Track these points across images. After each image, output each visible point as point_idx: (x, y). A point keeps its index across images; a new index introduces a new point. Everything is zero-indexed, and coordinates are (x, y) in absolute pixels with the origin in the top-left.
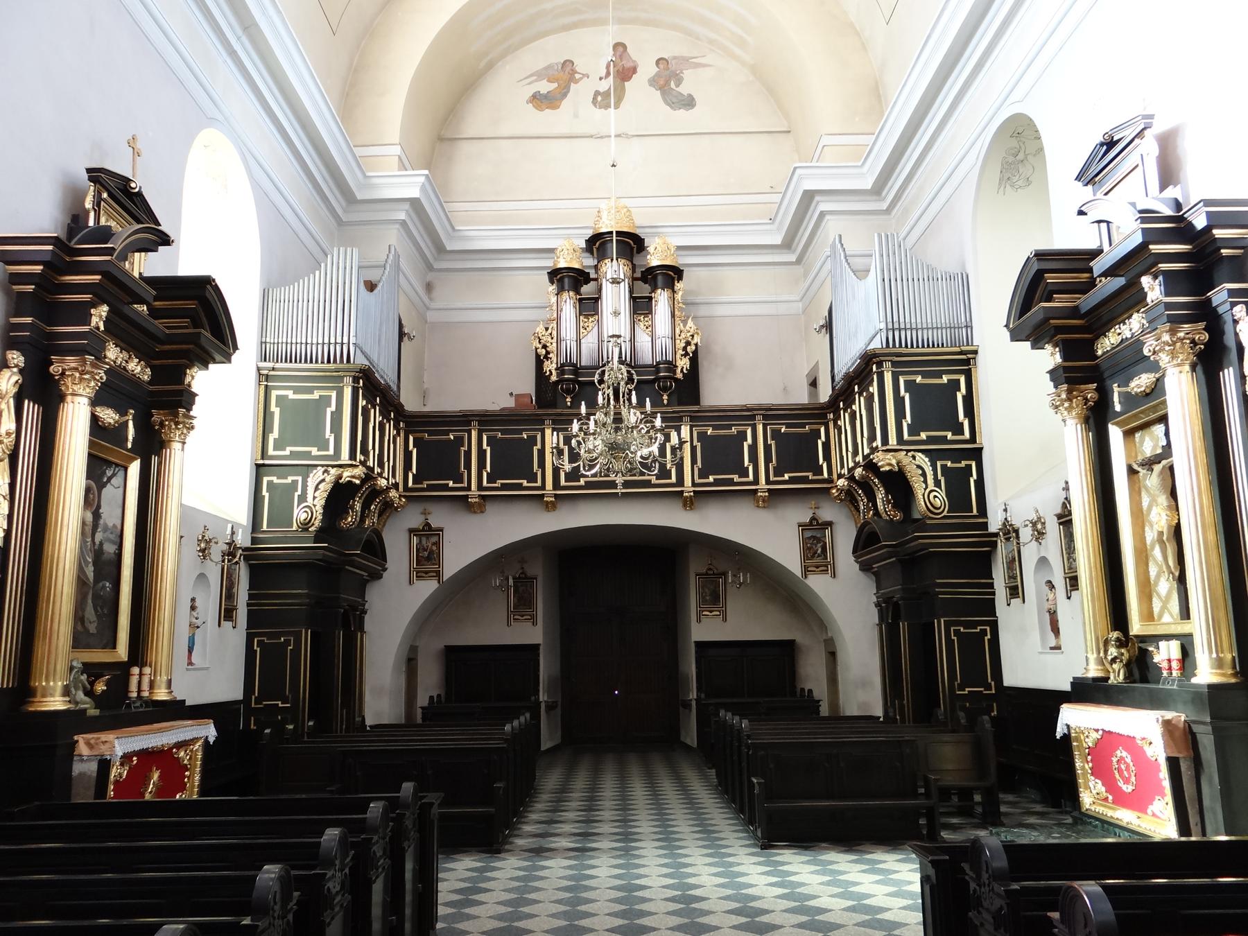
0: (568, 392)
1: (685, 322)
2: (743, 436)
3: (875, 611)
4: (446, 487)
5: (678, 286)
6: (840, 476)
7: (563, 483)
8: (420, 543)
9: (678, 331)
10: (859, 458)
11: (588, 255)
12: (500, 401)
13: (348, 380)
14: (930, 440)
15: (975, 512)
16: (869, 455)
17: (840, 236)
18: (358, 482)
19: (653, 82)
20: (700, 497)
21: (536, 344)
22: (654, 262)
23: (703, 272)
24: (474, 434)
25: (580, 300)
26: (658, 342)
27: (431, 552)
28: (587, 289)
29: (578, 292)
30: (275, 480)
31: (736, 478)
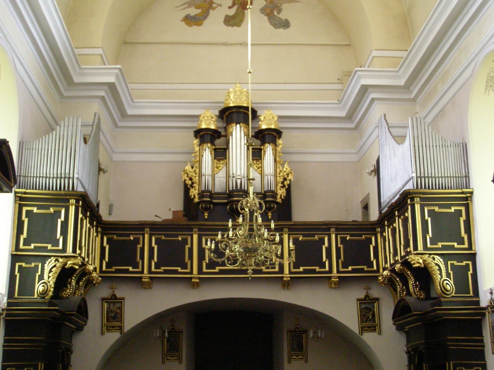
0: (206, 209)
1: (283, 165)
2: (322, 241)
3: (405, 357)
4: (127, 271)
5: (280, 142)
6: (384, 269)
7: (205, 270)
8: (109, 307)
9: (278, 171)
10: (398, 258)
11: (220, 120)
12: (165, 215)
13: (73, 201)
14: (444, 248)
15: (471, 294)
16: (405, 256)
17: (385, 115)
18: (77, 267)
19: (263, 11)
20: (295, 281)
21: (185, 177)
22: (264, 127)
23: (296, 133)
24: (147, 236)
25: (215, 149)
26: (266, 178)
27: (117, 313)
28: (219, 142)
29: (213, 144)
30: (24, 265)
31: (317, 269)
